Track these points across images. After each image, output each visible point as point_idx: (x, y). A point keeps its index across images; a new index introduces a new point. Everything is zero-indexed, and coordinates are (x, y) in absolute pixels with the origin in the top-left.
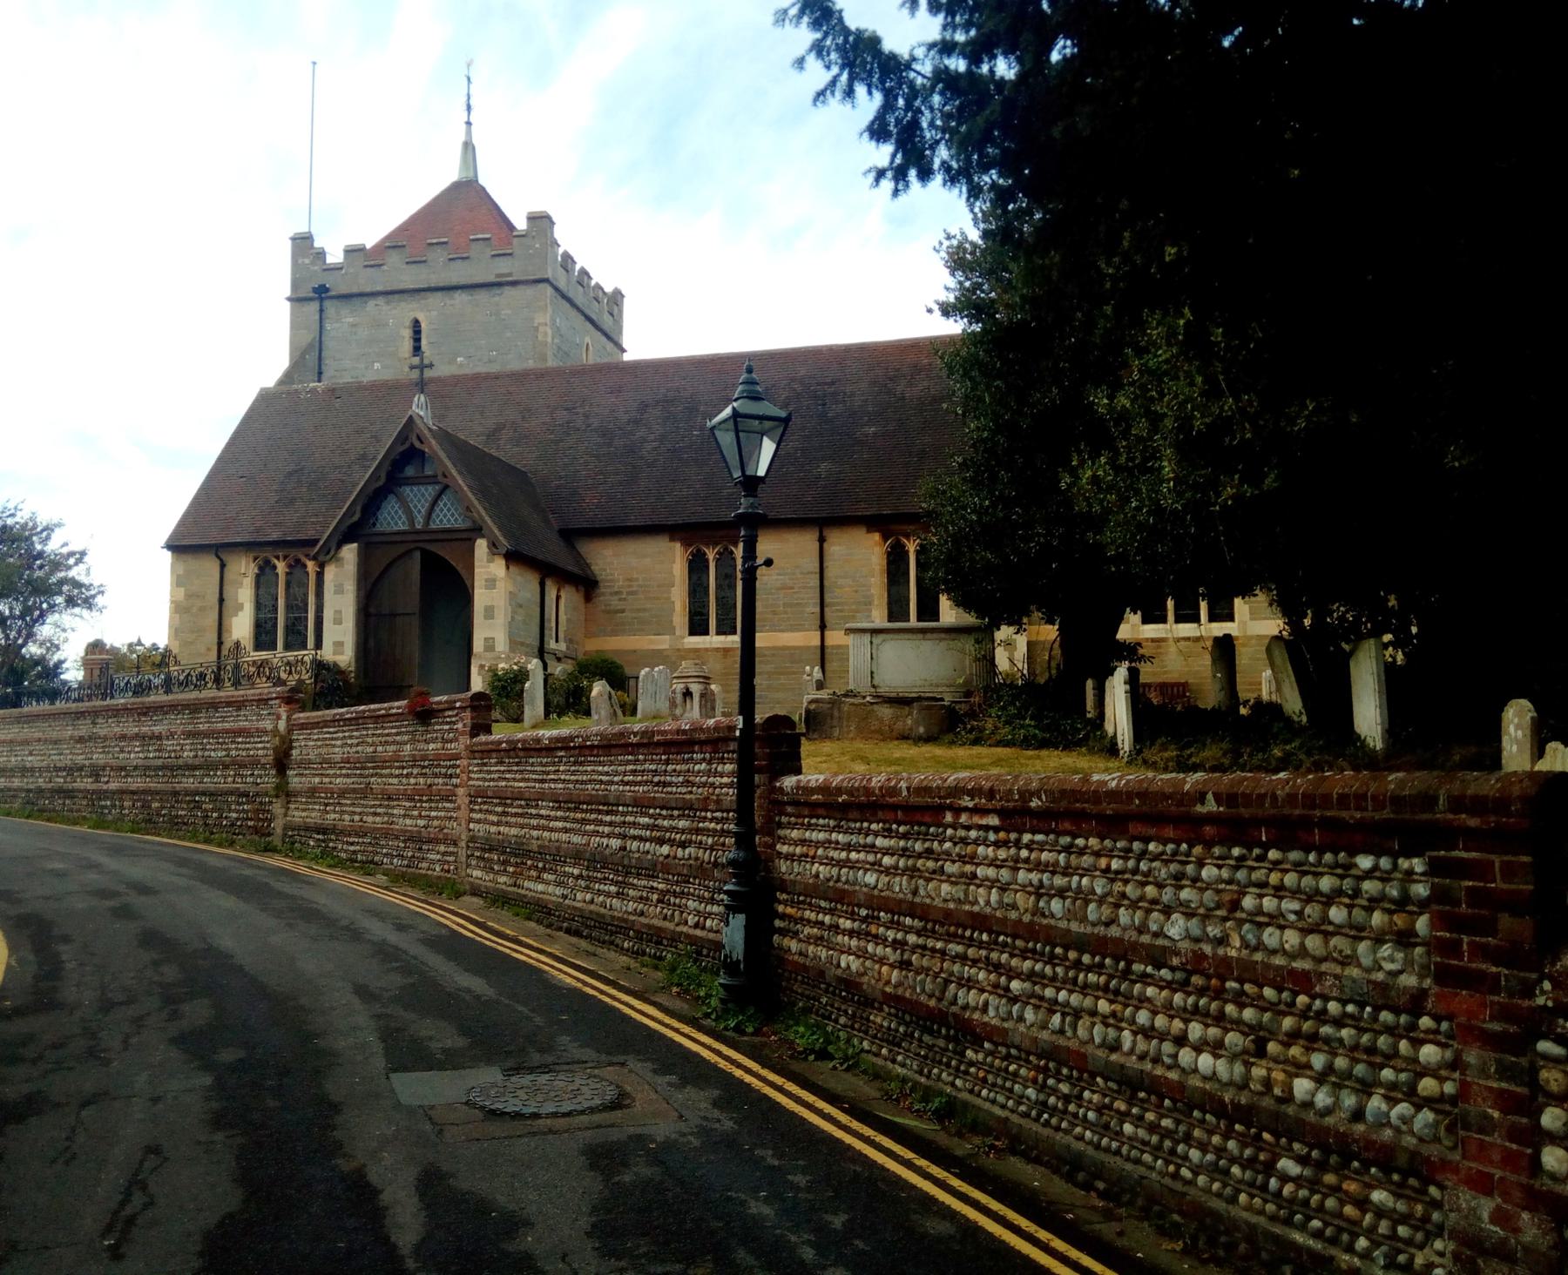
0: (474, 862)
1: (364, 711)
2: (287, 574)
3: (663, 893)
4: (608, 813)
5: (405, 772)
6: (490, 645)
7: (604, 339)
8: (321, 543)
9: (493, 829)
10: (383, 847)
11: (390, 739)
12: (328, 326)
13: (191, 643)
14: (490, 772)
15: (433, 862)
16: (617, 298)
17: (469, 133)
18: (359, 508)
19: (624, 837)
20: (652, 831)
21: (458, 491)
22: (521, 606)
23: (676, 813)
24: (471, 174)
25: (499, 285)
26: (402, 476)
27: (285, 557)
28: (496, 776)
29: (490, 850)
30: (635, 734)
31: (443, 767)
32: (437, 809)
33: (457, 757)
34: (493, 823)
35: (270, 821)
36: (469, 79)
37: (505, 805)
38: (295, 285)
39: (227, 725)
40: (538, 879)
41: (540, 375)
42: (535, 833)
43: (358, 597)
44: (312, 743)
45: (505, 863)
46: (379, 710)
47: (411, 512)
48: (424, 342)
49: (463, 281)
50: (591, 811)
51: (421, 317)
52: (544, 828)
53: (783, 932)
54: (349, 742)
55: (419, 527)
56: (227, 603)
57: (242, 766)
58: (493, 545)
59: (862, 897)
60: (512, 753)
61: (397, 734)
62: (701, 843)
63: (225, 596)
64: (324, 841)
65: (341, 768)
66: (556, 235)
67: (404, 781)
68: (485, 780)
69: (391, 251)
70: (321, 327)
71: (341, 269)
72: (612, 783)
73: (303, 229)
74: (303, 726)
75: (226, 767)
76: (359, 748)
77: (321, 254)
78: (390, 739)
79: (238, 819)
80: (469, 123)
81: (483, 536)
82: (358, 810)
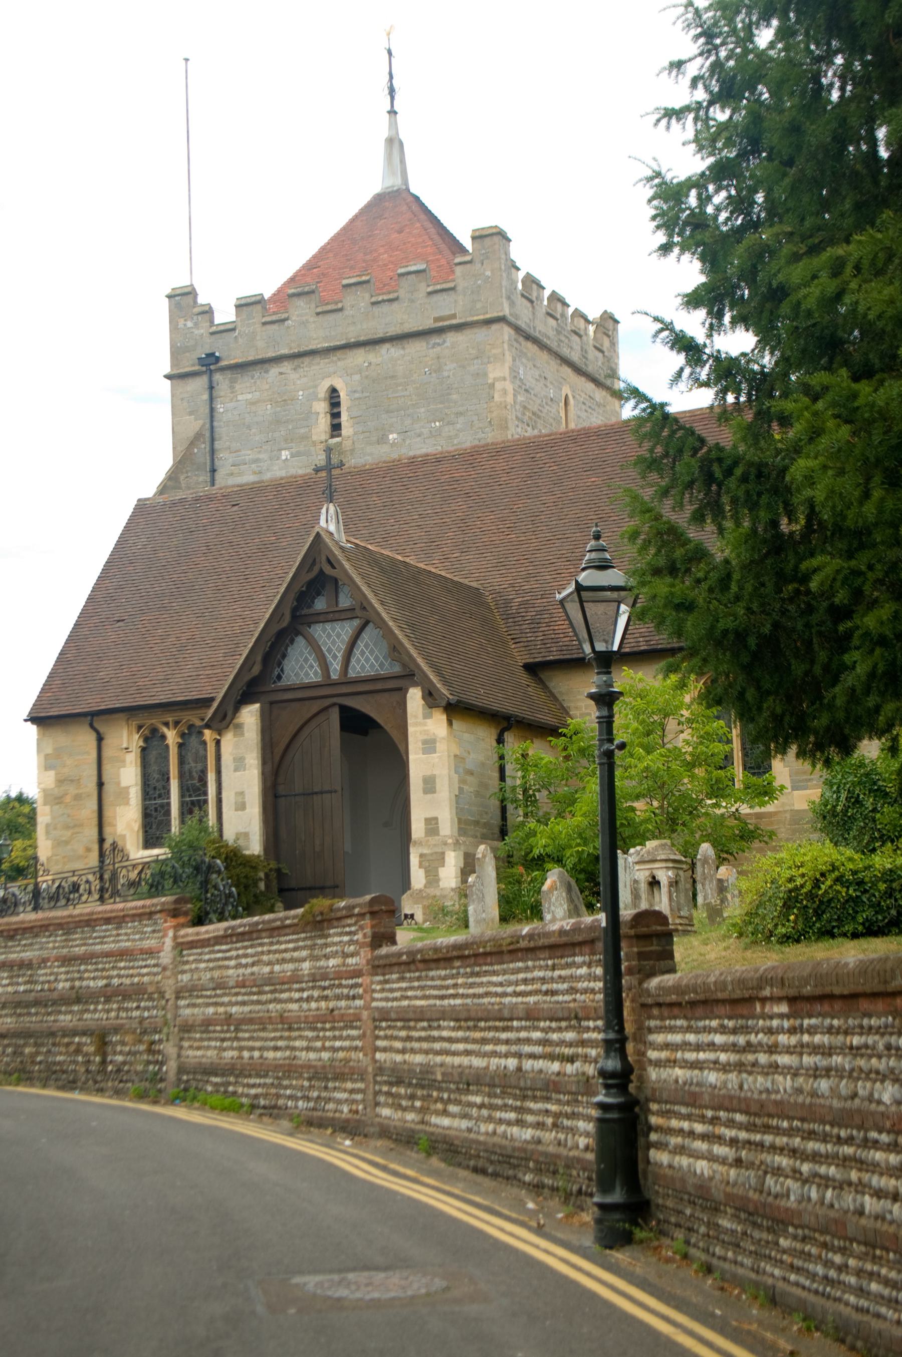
0: (382, 1099)
1: (257, 923)
2: (180, 746)
3: (557, 1115)
4: (505, 1029)
5: (305, 995)
6: (432, 825)
7: (590, 386)
8: (215, 705)
9: (399, 1058)
10: (286, 1088)
11: (287, 955)
12: (220, 408)
13: (67, 843)
14: (392, 990)
15: (339, 1102)
16: (605, 312)
17: (393, 125)
18: (259, 658)
19: (519, 1055)
20: (544, 1046)
21: (381, 624)
22: (471, 773)
23: (564, 1024)
24: (397, 182)
25: (440, 331)
26: (311, 611)
27: (176, 723)
28: (397, 994)
29: (399, 1082)
30: (524, 937)
31: (346, 986)
32: (341, 1038)
33: (358, 974)
34: (398, 1051)
35: (162, 1064)
36: (390, 53)
37: (409, 1028)
38: (176, 352)
39: (106, 947)
40: (445, 1113)
41: (498, 451)
42: (439, 1059)
43: (263, 773)
44: (203, 965)
45: (412, 1097)
46: (274, 920)
47: (324, 656)
48: (344, 417)
49: (393, 331)
50: (489, 1029)
51: (339, 385)
52: (448, 1053)
53: (660, 1146)
54: (244, 961)
55: (334, 676)
56: (108, 788)
57: (126, 996)
58: (430, 697)
59: (706, 1097)
60: (413, 967)
61: (295, 949)
62: (586, 1056)
63: (105, 778)
64: (222, 1084)
65: (237, 994)
66: (513, 256)
67: (305, 1005)
68: (387, 999)
69: (295, 299)
70: (212, 410)
71: (234, 330)
72: (505, 994)
73: (182, 281)
74: (192, 945)
75: (108, 1000)
76: (255, 969)
77: (208, 312)
78: (287, 955)
79: (124, 1063)
80: (393, 112)
81: (415, 685)
82: (258, 1044)
